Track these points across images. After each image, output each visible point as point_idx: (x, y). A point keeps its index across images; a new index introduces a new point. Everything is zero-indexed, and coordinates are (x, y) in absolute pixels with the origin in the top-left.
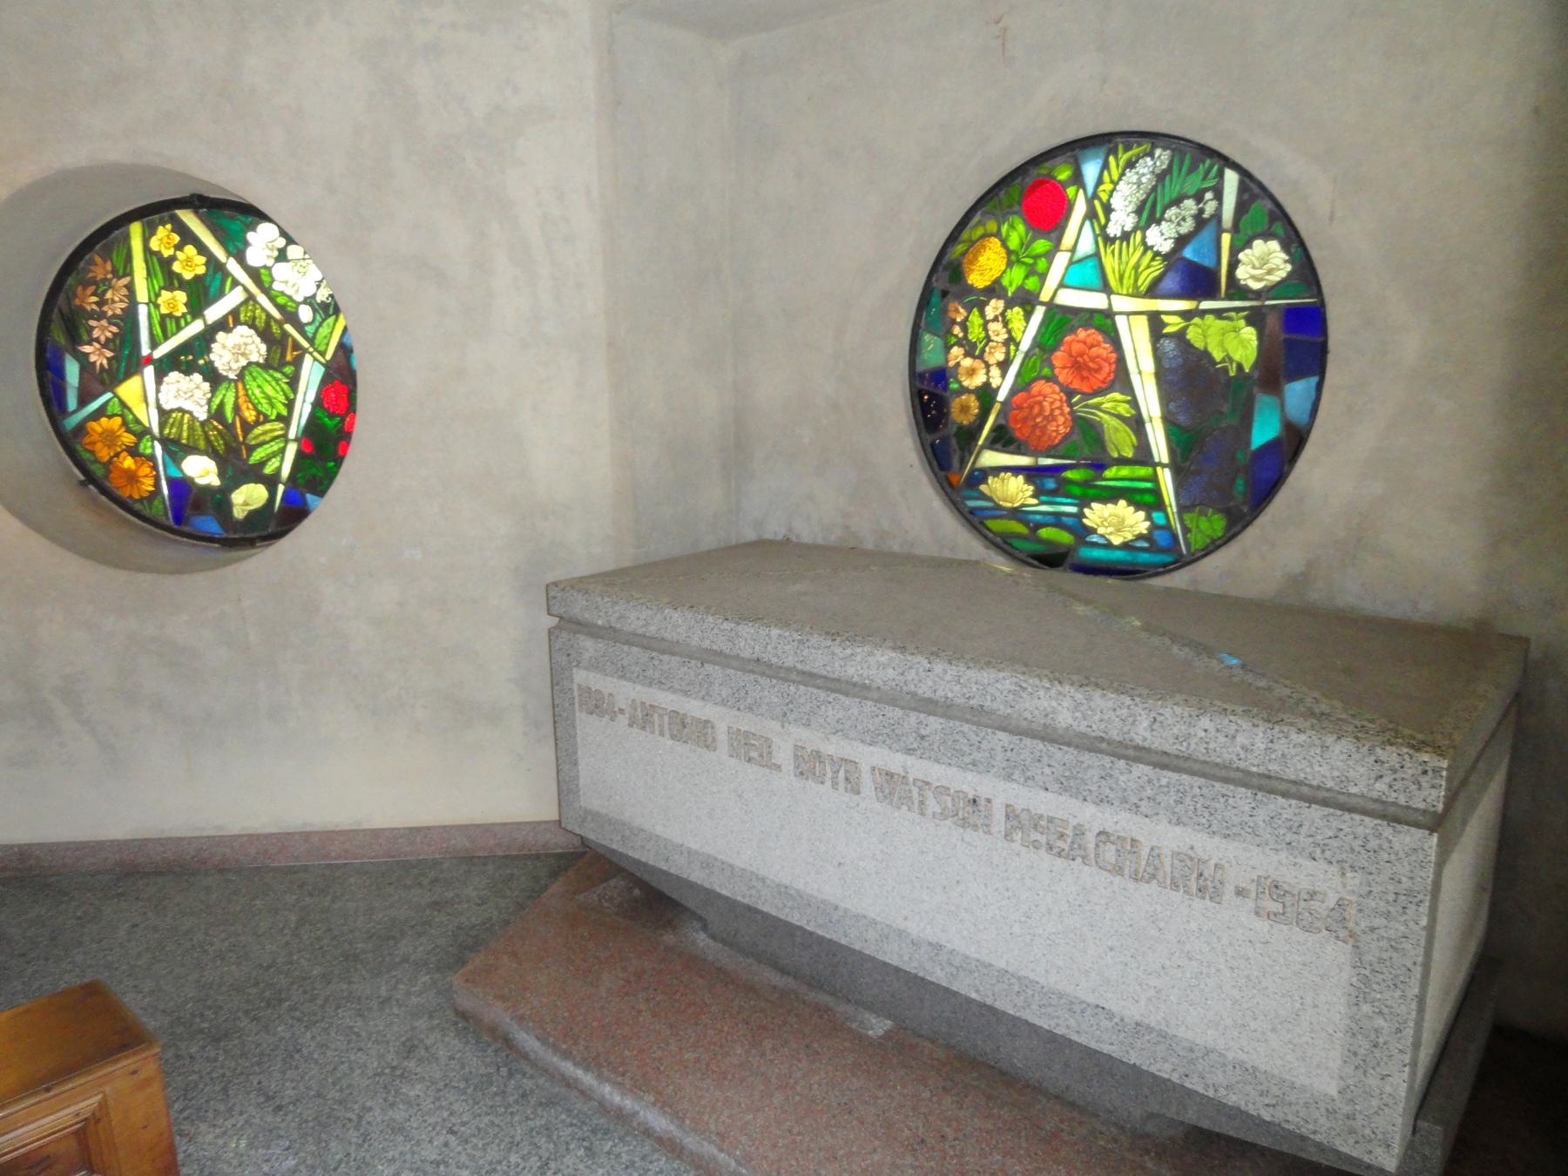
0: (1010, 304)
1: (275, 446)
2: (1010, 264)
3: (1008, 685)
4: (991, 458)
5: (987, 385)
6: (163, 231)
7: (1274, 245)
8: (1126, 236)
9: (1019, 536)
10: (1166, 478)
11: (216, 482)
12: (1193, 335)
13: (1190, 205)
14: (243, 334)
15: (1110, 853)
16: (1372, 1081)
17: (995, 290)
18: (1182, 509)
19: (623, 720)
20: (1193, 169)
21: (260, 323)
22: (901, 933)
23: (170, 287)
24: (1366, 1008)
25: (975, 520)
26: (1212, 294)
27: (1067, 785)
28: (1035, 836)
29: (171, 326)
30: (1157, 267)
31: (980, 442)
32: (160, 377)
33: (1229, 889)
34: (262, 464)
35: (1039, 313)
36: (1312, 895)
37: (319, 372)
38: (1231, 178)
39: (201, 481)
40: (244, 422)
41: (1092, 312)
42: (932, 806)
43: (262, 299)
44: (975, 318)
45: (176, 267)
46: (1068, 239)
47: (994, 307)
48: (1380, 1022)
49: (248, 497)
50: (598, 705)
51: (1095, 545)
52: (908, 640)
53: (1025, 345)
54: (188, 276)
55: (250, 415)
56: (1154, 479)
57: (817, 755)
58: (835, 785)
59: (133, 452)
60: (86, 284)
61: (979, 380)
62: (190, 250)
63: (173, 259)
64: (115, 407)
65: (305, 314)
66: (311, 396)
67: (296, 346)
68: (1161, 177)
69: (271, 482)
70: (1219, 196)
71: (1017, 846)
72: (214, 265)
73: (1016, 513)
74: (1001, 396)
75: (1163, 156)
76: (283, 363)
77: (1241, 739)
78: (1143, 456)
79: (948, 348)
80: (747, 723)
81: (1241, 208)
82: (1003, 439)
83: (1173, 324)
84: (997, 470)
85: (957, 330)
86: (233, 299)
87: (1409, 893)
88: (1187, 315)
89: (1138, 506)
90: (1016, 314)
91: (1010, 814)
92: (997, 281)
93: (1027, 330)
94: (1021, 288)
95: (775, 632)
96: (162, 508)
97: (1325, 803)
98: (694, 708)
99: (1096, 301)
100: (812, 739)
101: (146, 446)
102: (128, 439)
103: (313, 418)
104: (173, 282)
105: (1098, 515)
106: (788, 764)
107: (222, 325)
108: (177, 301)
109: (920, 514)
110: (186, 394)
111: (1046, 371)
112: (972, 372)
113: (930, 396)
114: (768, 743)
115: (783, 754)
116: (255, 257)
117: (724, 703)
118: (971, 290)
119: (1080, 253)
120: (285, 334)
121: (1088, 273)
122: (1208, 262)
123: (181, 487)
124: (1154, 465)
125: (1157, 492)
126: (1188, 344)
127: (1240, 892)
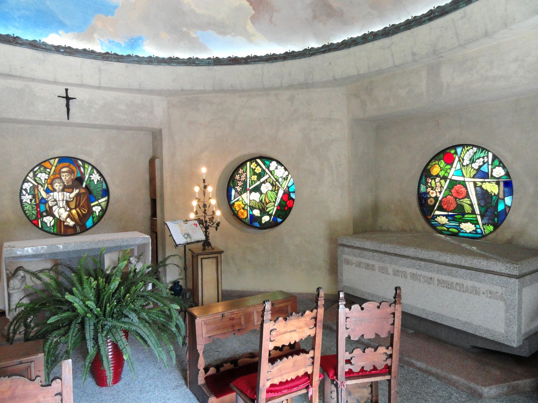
0: (441, 179)
1: (273, 207)
2: (441, 170)
3: (437, 255)
4: (437, 213)
5: (436, 196)
6: (254, 163)
7: (501, 168)
8: (467, 165)
9: (445, 230)
10: (479, 218)
11: (259, 215)
12: (484, 186)
13: (481, 160)
14: (268, 184)
15: (458, 287)
16: (510, 329)
17: (438, 176)
18: (483, 224)
19: (354, 265)
20: (482, 152)
21: (271, 182)
22: (416, 307)
23: (254, 175)
24: (508, 314)
25: (434, 227)
26: (488, 178)
27: (449, 274)
28: (443, 285)
29: (253, 182)
30: (475, 172)
31: (435, 208)
32: (250, 193)
33: (481, 293)
34: (269, 212)
35: (448, 181)
36: (497, 292)
37: (283, 192)
38: (490, 155)
39: (256, 215)
40: (266, 203)
41: (460, 181)
42: (422, 280)
43: (272, 177)
44: (433, 182)
45: (256, 171)
46: (454, 165)
47: (438, 179)
48: (511, 317)
49: (266, 219)
50: (348, 262)
51: (463, 232)
52: (418, 246)
53: (445, 188)
54: (258, 172)
55: (268, 201)
56: (476, 218)
57: (398, 271)
58: (402, 277)
59: (243, 208)
60: (238, 174)
61: (434, 195)
62: (258, 167)
63: (255, 169)
64: (241, 199)
65: (280, 180)
66: (280, 197)
67: (278, 187)
68: (475, 153)
69: (270, 215)
70: (488, 157)
71: (440, 287)
72: (263, 171)
73: (443, 225)
74: (440, 199)
75: (475, 149)
76: (275, 190)
77: (482, 263)
78: (473, 212)
79: (427, 188)
80: (382, 265)
81: (493, 161)
82: (440, 208)
83: (479, 184)
84: (439, 216)
85: (429, 184)
86: (266, 177)
87: (514, 291)
88: (482, 182)
89: (473, 224)
90: (443, 181)
91: (438, 280)
92: (438, 174)
93: (446, 185)
94: (444, 176)
95: (389, 246)
96: (248, 221)
97: (498, 275)
98: (371, 262)
99: (461, 179)
100: (397, 267)
101: (246, 208)
102: (243, 206)
103: (280, 201)
104: (255, 174)
105: (463, 226)
106: (391, 273)
107: (264, 182)
108: (255, 178)
109: (420, 223)
110: (256, 196)
111: (450, 194)
112: (433, 193)
113: (422, 198)
114: (387, 269)
115: (390, 271)
116: (271, 169)
117: (377, 261)
118: (432, 175)
119: (457, 168)
120: (276, 184)
121: (459, 173)
122: (486, 171)
123: (252, 216)
124: (476, 215)
125: (477, 220)
126: (482, 189)
127: (483, 293)
